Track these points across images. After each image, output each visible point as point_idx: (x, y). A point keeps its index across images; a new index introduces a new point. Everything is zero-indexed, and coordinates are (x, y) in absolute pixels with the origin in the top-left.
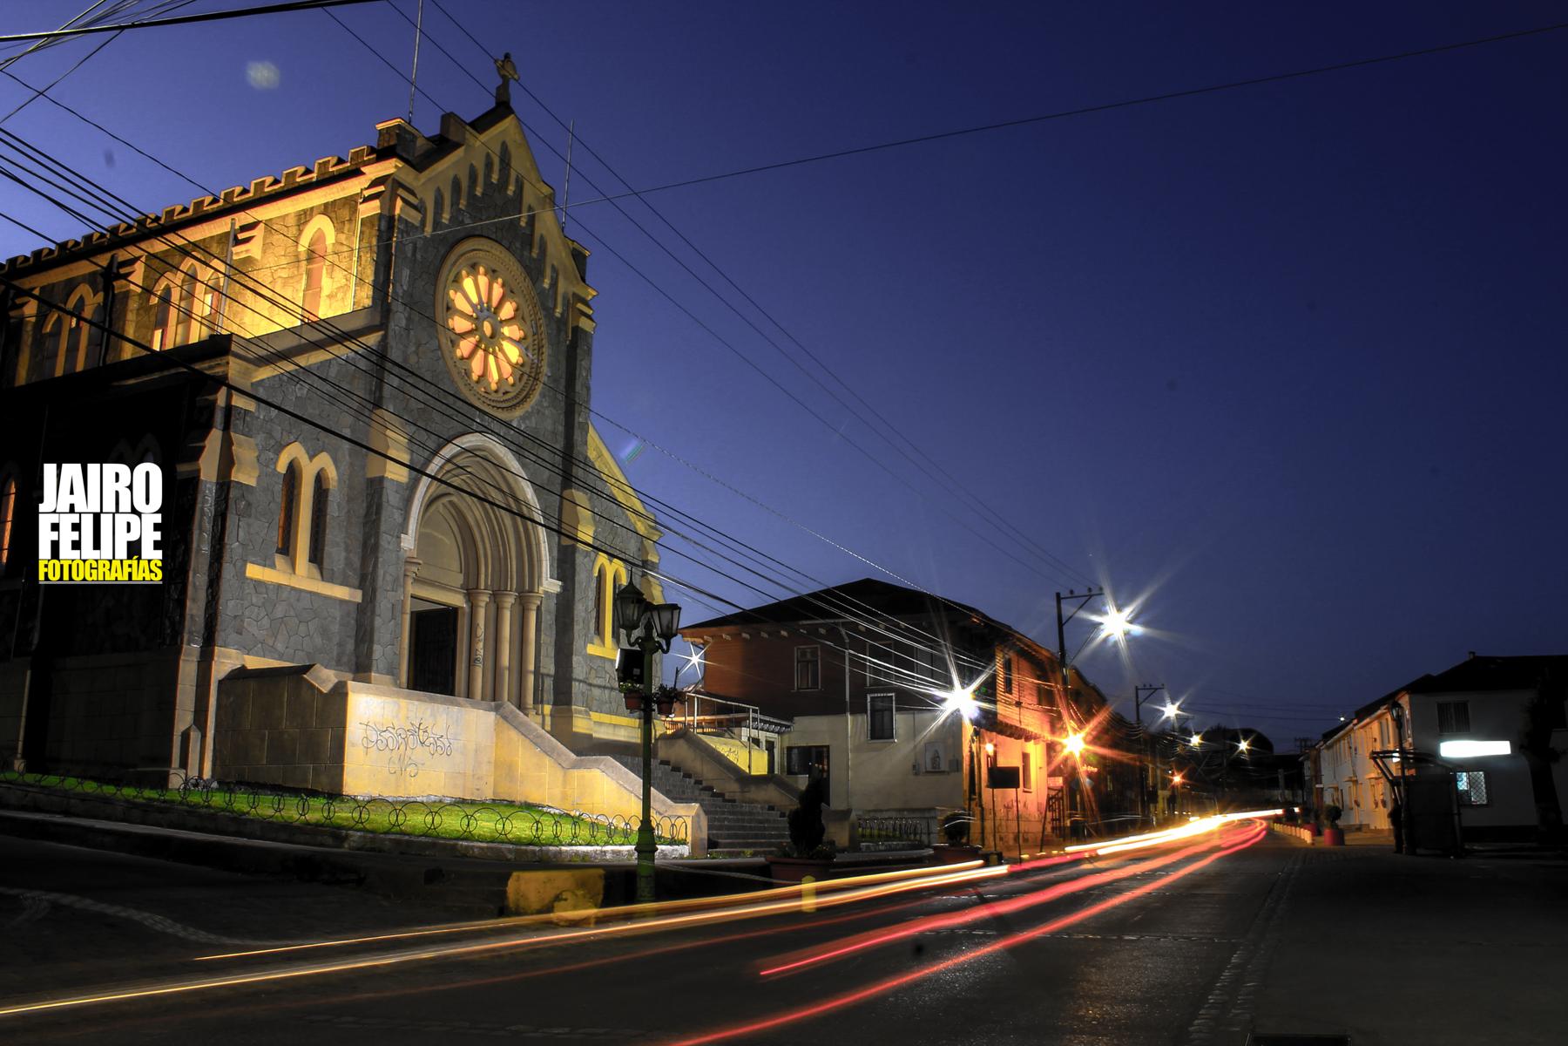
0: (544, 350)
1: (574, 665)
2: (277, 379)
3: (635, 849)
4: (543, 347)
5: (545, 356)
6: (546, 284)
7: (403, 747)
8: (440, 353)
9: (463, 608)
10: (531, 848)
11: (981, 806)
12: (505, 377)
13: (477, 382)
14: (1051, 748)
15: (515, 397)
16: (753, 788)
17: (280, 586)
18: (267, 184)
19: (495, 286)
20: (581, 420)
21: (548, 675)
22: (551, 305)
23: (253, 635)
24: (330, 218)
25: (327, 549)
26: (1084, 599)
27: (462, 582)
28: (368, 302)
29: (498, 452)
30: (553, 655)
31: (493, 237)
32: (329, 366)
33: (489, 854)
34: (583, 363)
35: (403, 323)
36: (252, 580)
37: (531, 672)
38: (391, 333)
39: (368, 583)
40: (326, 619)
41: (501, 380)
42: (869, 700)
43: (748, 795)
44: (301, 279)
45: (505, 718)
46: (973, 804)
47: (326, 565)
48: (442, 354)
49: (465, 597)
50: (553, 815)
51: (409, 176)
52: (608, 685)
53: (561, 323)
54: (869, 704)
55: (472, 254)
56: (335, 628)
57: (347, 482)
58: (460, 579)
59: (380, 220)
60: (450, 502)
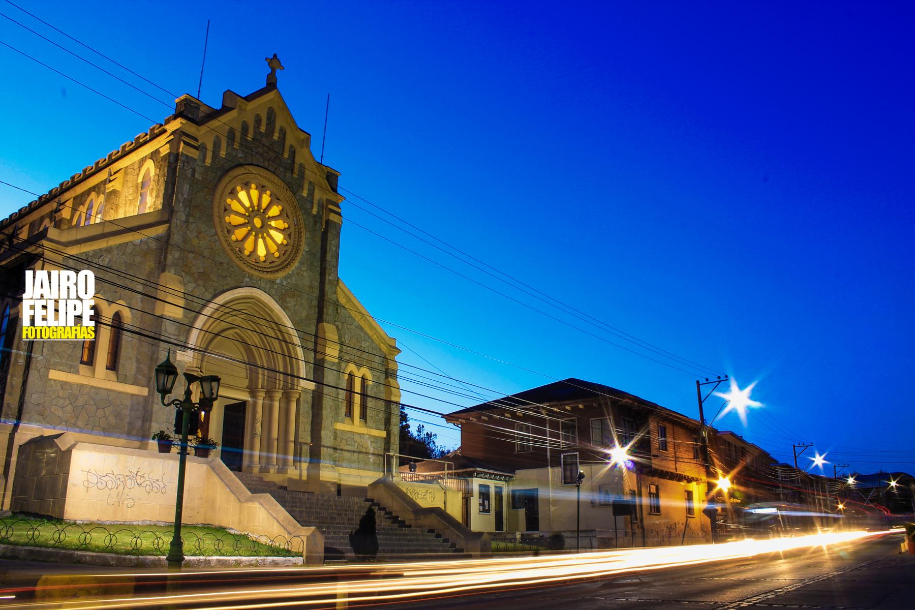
0: (302, 235)
1: (323, 437)
2: (84, 254)
3: (167, 559)
4: (301, 233)
5: (303, 239)
6: (305, 194)
7: (121, 487)
8: (216, 237)
9: (248, 401)
10: (129, 556)
11: (643, 528)
12: (272, 252)
13: (249, 256)
14: (710, 486)
15: (279, 265)
16: (422, 517)
17: (82, 385)
18: (127, 146)
19: (264, 196)
20: (331, 278)
21: (306, 444)
22: (308, 206)
23: (59, 417)
24: (153, 161)
25: (121, 361)
26: (718, 383)
27: (247, 385)
28: (160, 207)
29: (263, 299)
30: (309, 430)
31: (262, 165)
32: (126, 247)
33: (97, 561)
34: (333, 242)
35: (184, 218)
36: (55, 380)
37: (292, 441)
38: (173, 225)
39: (151, 383)
40: (119, 406)
41: (269, 254)
42: (562, 457)
43: (419, 522)
44: (138, 199)
45: (213, 468)
46: (635, 526)
47: (120, 371)
48: (219, 238)
49: (249, 393)
50: (234, 535)
51: (192, 129)
52: (357, 450)
53: (317, 218)
54: (562, 460)
55: (244, 176)
56: (126, 412)
57: (140, 319)
58: (246, 382)
59: (169, 156)
60: (236, 333)
